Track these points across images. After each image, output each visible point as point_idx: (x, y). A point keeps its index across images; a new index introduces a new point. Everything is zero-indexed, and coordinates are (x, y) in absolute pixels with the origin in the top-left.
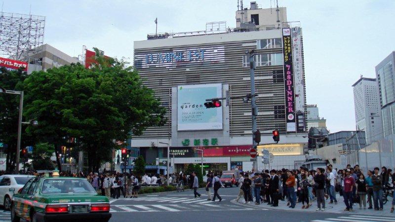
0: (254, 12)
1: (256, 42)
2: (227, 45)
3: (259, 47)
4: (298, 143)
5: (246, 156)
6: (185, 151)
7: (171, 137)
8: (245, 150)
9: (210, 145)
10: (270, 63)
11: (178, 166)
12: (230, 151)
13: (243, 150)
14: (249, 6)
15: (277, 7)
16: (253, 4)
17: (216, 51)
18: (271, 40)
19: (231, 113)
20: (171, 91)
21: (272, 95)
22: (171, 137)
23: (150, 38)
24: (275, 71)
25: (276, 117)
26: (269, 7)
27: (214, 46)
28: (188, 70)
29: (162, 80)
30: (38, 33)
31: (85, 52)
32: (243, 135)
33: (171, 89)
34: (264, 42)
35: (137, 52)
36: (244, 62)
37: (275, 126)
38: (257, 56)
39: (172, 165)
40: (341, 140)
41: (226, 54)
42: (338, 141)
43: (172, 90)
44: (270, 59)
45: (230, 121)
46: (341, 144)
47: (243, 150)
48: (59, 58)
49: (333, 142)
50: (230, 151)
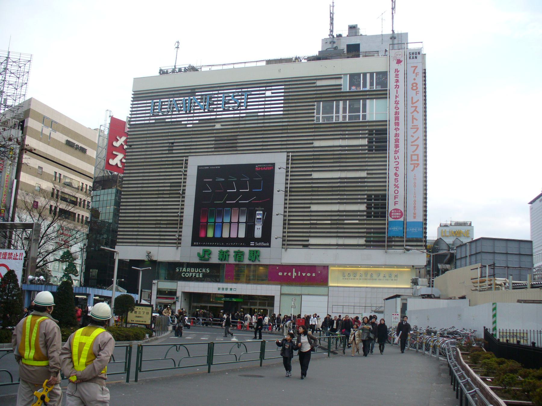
0: (353, 41)
1: (341, 78)
2: (287, 83)
3: (346, 88)
4: (408, 267)
5: (308, 285)
6: (204, 270)
7: (180, 243)
8: (309, 275)
9: (246, 261)
10: (364, 117)
11: (191, 297)
12: (280, 274)
13: (285, 274)
14: (345, 33)
15: (393, 31)
16: (353, 29)
17: (268, 93)
18: (368, 76)
19: (288, 202)
20: (186, 164)
21: (364, 174)
22: (180, 243)
23: (163, 72)
24: (372, 130)
25: (369, 215)
26: (380, 33)
27: (268, 84)
28: (218, 126)
29: (173, 143)
30: (20, 81)
31: (109, 121)
32: (306, 246)
33: (187, 160)
34: (354, 78)
35: (138, 96)
36: (318, 113)
37: (367, 233)
38: (341, 103)
39: (179, 294)
40: (479, 256)
41: (287, 100)
42: (473, 258)
43: (189, 162)
44: (364, 110)
45: (285, 220)
46: (479, 265)
47: (304, 274)
48: (56, 123)
49: (463, 261)
50: (280, 274)
